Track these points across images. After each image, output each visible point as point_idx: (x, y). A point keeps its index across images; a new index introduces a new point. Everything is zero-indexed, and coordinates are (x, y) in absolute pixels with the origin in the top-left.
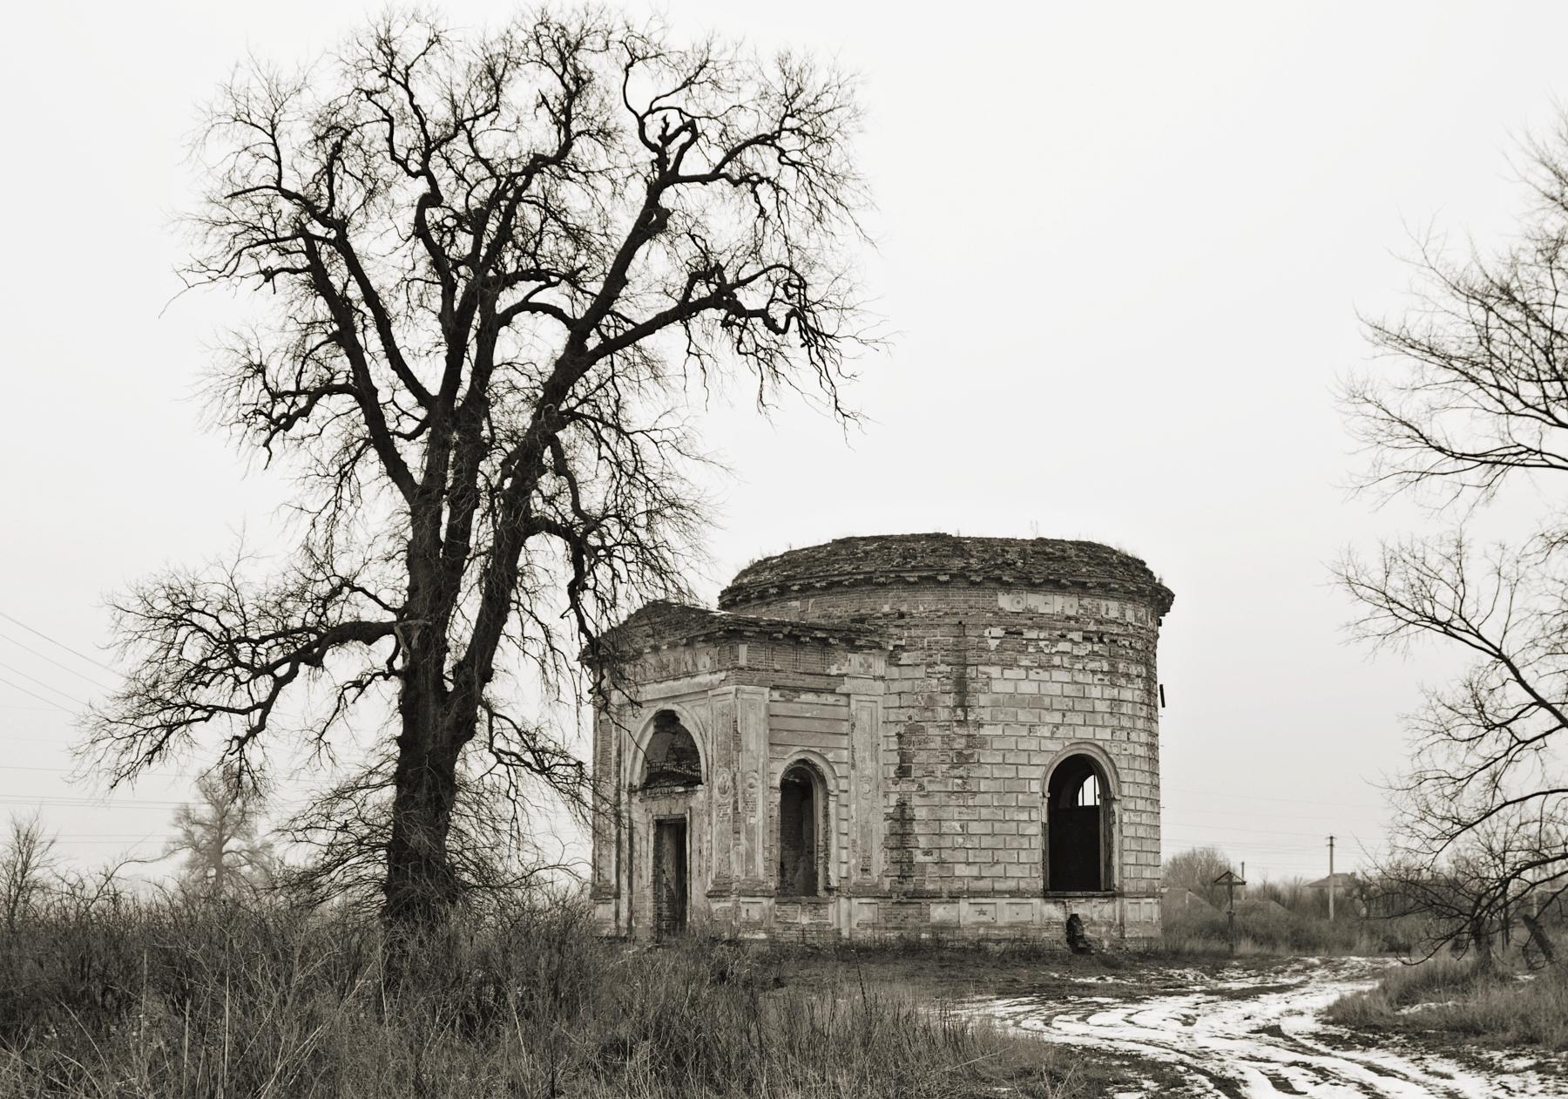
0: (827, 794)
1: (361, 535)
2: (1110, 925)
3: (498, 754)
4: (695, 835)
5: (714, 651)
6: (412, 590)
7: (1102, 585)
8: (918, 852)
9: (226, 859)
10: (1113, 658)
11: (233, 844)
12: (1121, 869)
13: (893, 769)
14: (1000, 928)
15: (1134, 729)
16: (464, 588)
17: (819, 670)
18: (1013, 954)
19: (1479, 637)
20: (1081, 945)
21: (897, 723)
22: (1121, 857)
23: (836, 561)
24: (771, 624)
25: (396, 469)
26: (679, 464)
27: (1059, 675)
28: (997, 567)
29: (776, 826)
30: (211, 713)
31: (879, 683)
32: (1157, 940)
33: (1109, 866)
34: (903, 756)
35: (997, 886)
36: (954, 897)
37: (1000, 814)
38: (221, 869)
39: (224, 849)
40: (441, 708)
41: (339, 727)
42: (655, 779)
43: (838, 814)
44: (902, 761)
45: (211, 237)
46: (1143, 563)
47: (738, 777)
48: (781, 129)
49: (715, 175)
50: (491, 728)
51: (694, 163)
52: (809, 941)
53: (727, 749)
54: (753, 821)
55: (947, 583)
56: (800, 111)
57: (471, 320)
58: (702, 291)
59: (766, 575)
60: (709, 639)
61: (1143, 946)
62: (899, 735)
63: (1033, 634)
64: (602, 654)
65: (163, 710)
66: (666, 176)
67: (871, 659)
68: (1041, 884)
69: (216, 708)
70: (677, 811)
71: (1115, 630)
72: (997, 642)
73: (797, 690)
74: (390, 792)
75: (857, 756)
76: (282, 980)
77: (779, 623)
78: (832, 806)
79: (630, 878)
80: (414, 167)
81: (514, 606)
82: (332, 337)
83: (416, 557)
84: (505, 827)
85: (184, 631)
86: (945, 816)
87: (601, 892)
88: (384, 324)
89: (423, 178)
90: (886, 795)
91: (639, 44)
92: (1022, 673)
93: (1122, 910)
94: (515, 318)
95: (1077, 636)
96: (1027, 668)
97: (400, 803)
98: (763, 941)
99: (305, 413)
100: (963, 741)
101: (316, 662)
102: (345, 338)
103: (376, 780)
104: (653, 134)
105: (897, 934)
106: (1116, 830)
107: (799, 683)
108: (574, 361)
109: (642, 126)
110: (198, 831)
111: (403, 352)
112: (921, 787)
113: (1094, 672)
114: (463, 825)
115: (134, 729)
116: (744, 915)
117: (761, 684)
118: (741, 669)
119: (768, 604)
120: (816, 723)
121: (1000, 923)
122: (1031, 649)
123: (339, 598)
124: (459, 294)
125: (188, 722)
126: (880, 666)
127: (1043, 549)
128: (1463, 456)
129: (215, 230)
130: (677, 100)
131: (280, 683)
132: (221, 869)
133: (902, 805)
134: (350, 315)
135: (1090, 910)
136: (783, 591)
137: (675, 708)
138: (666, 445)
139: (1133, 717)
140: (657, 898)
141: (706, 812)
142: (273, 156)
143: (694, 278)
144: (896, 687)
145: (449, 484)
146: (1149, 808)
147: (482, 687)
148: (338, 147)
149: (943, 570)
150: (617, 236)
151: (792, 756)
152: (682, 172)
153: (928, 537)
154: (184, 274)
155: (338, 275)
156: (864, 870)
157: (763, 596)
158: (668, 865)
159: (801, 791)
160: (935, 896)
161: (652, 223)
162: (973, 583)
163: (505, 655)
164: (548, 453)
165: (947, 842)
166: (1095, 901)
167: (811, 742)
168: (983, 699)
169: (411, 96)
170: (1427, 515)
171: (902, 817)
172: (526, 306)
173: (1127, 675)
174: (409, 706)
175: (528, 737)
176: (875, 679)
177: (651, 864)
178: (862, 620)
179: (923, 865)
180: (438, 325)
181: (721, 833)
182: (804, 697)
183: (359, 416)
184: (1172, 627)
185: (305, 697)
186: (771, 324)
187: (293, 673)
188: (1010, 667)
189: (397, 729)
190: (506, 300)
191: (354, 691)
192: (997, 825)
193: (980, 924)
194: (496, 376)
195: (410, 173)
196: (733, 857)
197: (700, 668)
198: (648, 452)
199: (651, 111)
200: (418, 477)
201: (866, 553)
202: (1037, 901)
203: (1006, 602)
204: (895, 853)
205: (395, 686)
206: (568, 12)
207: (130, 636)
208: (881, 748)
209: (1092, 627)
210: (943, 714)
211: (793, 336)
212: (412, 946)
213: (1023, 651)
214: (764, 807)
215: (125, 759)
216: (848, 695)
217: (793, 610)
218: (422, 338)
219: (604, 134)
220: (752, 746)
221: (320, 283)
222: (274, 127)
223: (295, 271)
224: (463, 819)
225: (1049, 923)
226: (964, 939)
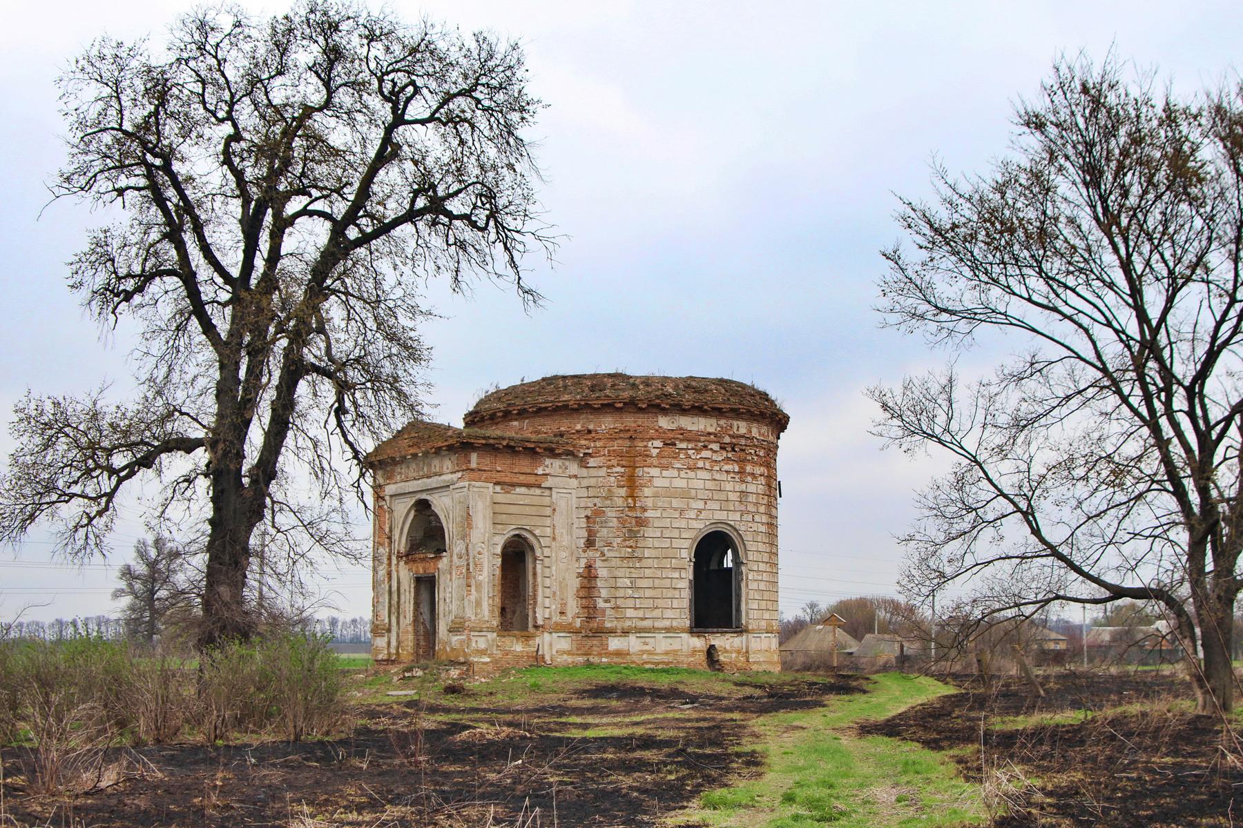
0: (535, 559)
2: (739, 652)
5: (454, 458)
12: (747, 614)
13: (583, 541)
17: (528, 471)
19: (962, 448)
22: (747, 604)
25: (208, 328)
27: (701, 474)
29: (498, 581)
30: (71, 498)
31: (573, 480)
33: (738, 610)
35: (656, 625)
36: (625, 633)
37: (658, 573)
40: (240, 500)
41: (168, 507)
44: (589, 536)
49: (431, 119)
51: (416, 109)
54: (480, 578)
57: (263, 211)
58: (421, 203)
66: (399, 119)
67: (567, 463)
68: (688, 622)
71: (743, 442)
73: (513, 485)
78: (539, 567)
79: (398, 618)
80: (221, 114)
82: (165, 236)
83: (224, 391)
90: (578, 559)
92: (675, 473)
93: (747, 641)
94: (297, 221)
95: (715, 447)
96: (679, 469)
104: (388, 86)
106: (743, 585)
107: (515, 480)
108: (338, 249)
111: (213, 248)
112: (603, 554)
121: (658, 651)
122: (682, 456)
126: (573, 468)
127: (690, 384)
133: (589, 567)
134: (182, 220)
135: (724, 642)
136: (507, 415)
137: (428, 497)
140: (416, 632)
141: (448, 570)
143: (416, 193)
144: (585, 483)
151: (509, 532)
152: (407, 117)
158: (425, 609)
159: (516, 557)
160: (612, 632)
161: (388, 153)
162: (641, 409)
163: (287, 461)
165: (621, 593)
170: (922, 360)
172: (304, 212)
176: (570, 477)
179: (604, 610)
182: (518, 490)
184: (787, 441)
185: (143, 489)
186: (474, 225)
188: (666, 468)
190: (295, 205)
193: (644, 652)
194: (284, 263)
200: (223, 336)
202: (685, 636)
203: (664, 422)
209: (727, 440)
210: (620, 502)
214: (489, 568)
216: (550, 489)
217: (516, 430)
218: (226, 237)
223: (139, 189)
226: (633, 662)
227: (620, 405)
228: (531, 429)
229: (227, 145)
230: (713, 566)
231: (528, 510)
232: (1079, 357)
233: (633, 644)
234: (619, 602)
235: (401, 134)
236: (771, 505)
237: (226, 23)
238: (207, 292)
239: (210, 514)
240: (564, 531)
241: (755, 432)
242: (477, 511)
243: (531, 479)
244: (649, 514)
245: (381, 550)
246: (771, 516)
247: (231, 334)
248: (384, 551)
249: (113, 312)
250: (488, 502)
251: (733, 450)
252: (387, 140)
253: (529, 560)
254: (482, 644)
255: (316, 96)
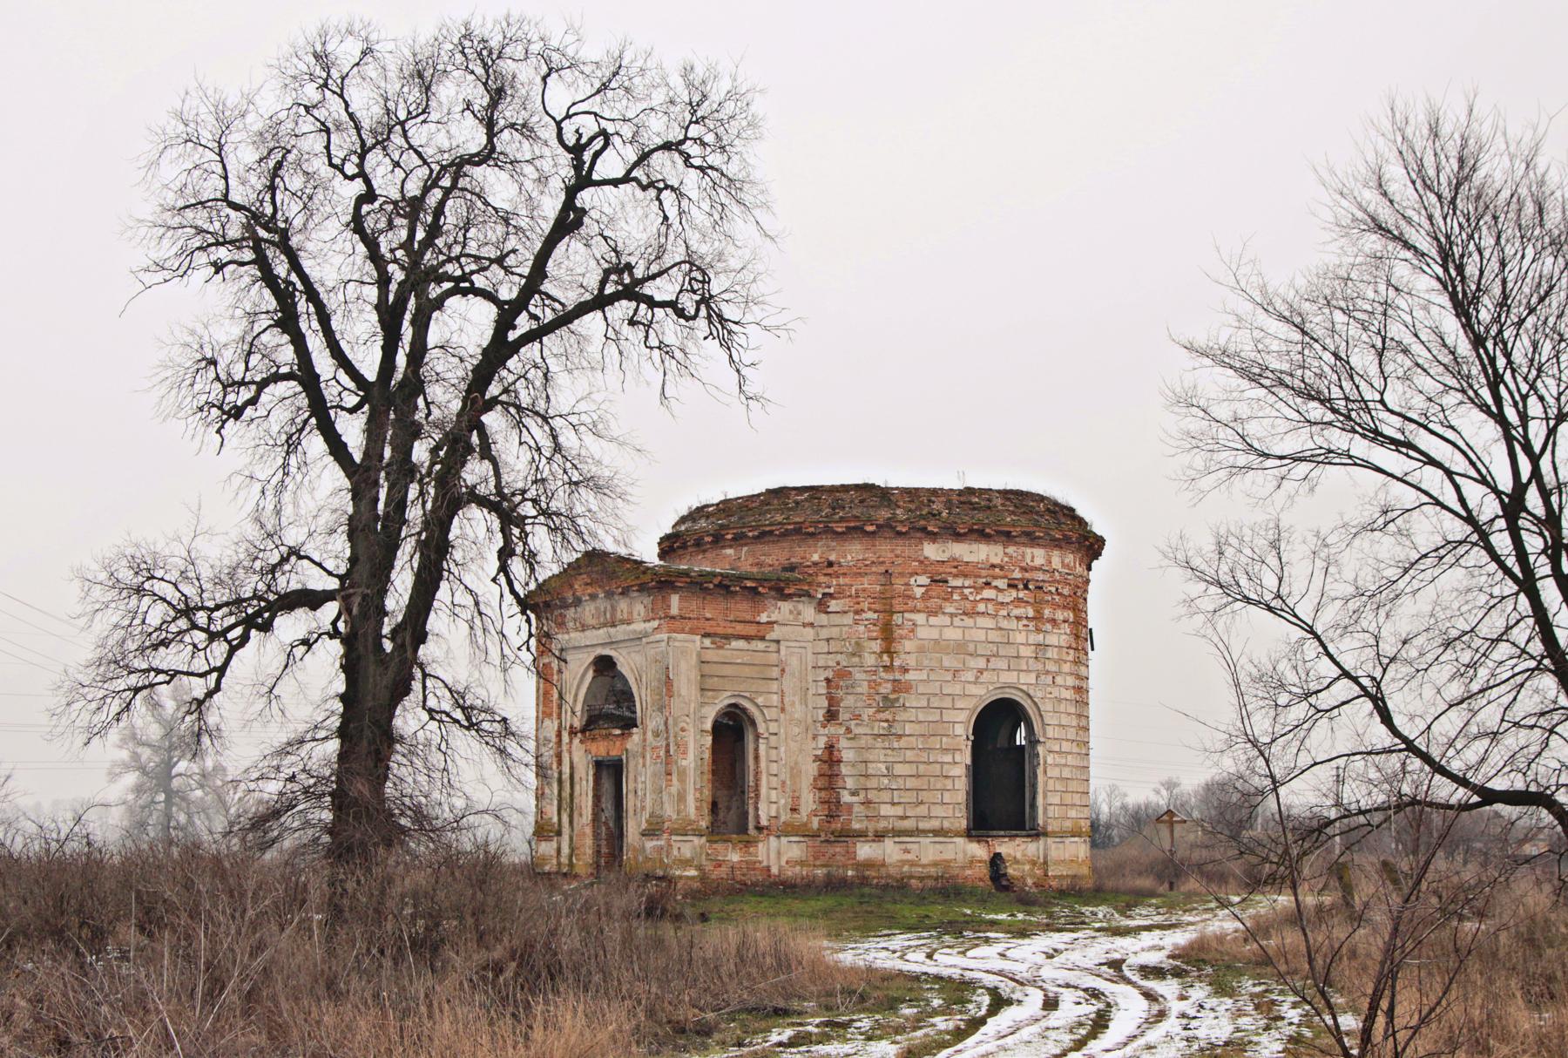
0: (757, 736)
1: (308, 504)
3: (430, 711)
4: (631, 776)
5: (648, 600)
6: (353, 560)
7: (1027, 534)
8: (845, 793)
9: (176, 783)
10: (1038, 605)
11: (182, 766)
13: (821, 713)
14: (924, 866)
15: (1059, 673)
16: (398, 564)
17: (748, 617)
18: (933, 890)
19: (1295, 616)
20: (1005, 883)
21: (826, 668)
22: (1045, 797)
23: (769, 511)
24: (701, 574)
25: (337, 448)
26: (593, 445)
27: (981, 621)
28: (922, 517)
29: (707, 768)
30: (173, 677)
32: (1081, 878)
33: (1033, 806)
34: (832, 700)
35: (922, 825)
36: (879, 836)
38: (170, 794)
39: (174, 772)
40: (380, 672)
41: (287, 693)
42: (593, 723)
43: (768, 754)
45: (165, 241)
46: (1073, 510)
47: (670, 721)
48: (686, 138)
49: (626, 179)
50: (424, 687)
51: (610, 165)
52: (739, 878)
53: (660, 694)
54: (684, 763)
55: (873, 533)
56: (703, 118)
57: (407, 301)
59: (703, 523)
60: (642, 588)
61: (1065, 884)
62: (828, 680)
63: (958, 582)
64: (541, 604)
65: (129, 671)
66: (584, 180)
67: (800, 606)
68: (964, 824)
69: (177, 672)
70: (614, 753)
71: (1040, 576)
72: (923, 590)
73: (727, 637)
74: (334, 745)
75: (786, 700)
76: (237, 915)
77: (709, 573)
78: (762, 748)
81: (446, 574)
82: (278, 324)
83: (356, 529)
84: (437, 775)
85: (146, 600)
86: (871, 758)
87: (543, 830)
88: (324, 318)
89: (359, 181)
90: (815, 737)
91: (555, 57)
92: (947, 620)
93: (1045, 849)
94: (448, 303)
95: (1002, 584)
96: (952, 615)
97: (343, 756)
98: (692, 878)
99: (253, 401)
100: (889, 686)
101: (266, 627)
102: (287, 322)
103: (321, 734)
105: (825, 870)
106: (1040, 771)
107: (730, 631)
108: (499, 351)
109: (560, 130)
110: (145, 753)
111: (343, 344)
112: (849, 730)
113: (1018, 618)
114: (403, 772)
115: (101, 694)
116: (675, 852)
117: (692, 632)
118: (673, 618)
119: (704, 551)
120: (747, 669)
121: (924, 861)
122: (956, 597)
123: (287, 567)
124: (393, 287)
125: (152, 685)
126: (808, 612)
128: (1281, 458)
129: (170, 234)
130: (594, 105)
131: (232, 651)
132: (170, 794)
133: (830, 748)
134: (292, 300)
135: (1009, 848)
136: (718, 539)
138: (582, 429)
139: (1058, 661)
140: (596, 835)
142: (219, 170)
144: (824, 633)
145: (383, 474)
146: (1076, 750)
147: (416, 650)
148: (279, 165)
149: (870, 521)
150: (544, 218)
151: (723, 701)
152: (595, 177)
153: (857, 487)
154: (141, 275)
155: (281, 268)
156: (793, 810)
157: (698, 543)
158: (608, 804)
159: (732, 732)
160: (861, 835)
161: (569, 222)
162: (899, 534)
163: (436, 622)
164: (475, 439)
165: (873, 783)
166: (1018, 840)
167: (742, 687)
168: (908, 645)
169: (347, 105)
170: (1244, 503)
171: (830, 759)
173: (1053, 621)
174: (350, 666)
175: (458, 697)
176: (804, 625)
177: (590, 803)
178: (792, 568)
179: (850, 806)
180: (374, 317)
181: (654, 775)
182: (735, 644)
183: (303, 401)
186: (680, 313)
187: (244, 639)
189: (340, 686)
191: (303, 649)
192: (921, 767)
193: (904, 862)
195: (346, 177)
196: (665, 798)
197: (635, 615)
198: (568, 439)
199: (568, 116)
200: (358, 457)
201: (797, 503)
202: (960, 841)
203: (931, 551)
204: (823, 794)
205: (335, 648)
206: (489, 25)
207: (97, 606)
208: (810, 692)
209: (1017, 574)
210: (870, 660)
211: (701, 324)
212: (350, 886)
213: (948, 598)
214: (696, 749)
215: (96, 719)
216: (778, 642)
217: (729, 560)
219: (525, 130)
220: (684, 692)
221: (269, 279)
222: (221, 147)
224: (399, 766)
225: (972, 862)
227: (870, 528)
228: (751, 561)
229: (357, 208)
230: (1002, 742)
231: (747, 671)
232: (1438, 503)
233: (890, 851)
234: (872, 795)
235: (585, 197)
236: (1080, 661)
237: (353, 49)
238: (330, 393)
239: (342, 688)
240: (797, 699)
241: (1056, 562)
242: (674, 664)
243: (751, 630)
244: (910, 676)
245: (547, 722)
246: (1078, 677)
247: (366, 454)
248: (551, 727)
249: (218, 432)
250: (694, 660)
251: (1026, 587)
252: (569, 204)
253: (749, 738)
254: (687, 852)
255: (472, 138)
